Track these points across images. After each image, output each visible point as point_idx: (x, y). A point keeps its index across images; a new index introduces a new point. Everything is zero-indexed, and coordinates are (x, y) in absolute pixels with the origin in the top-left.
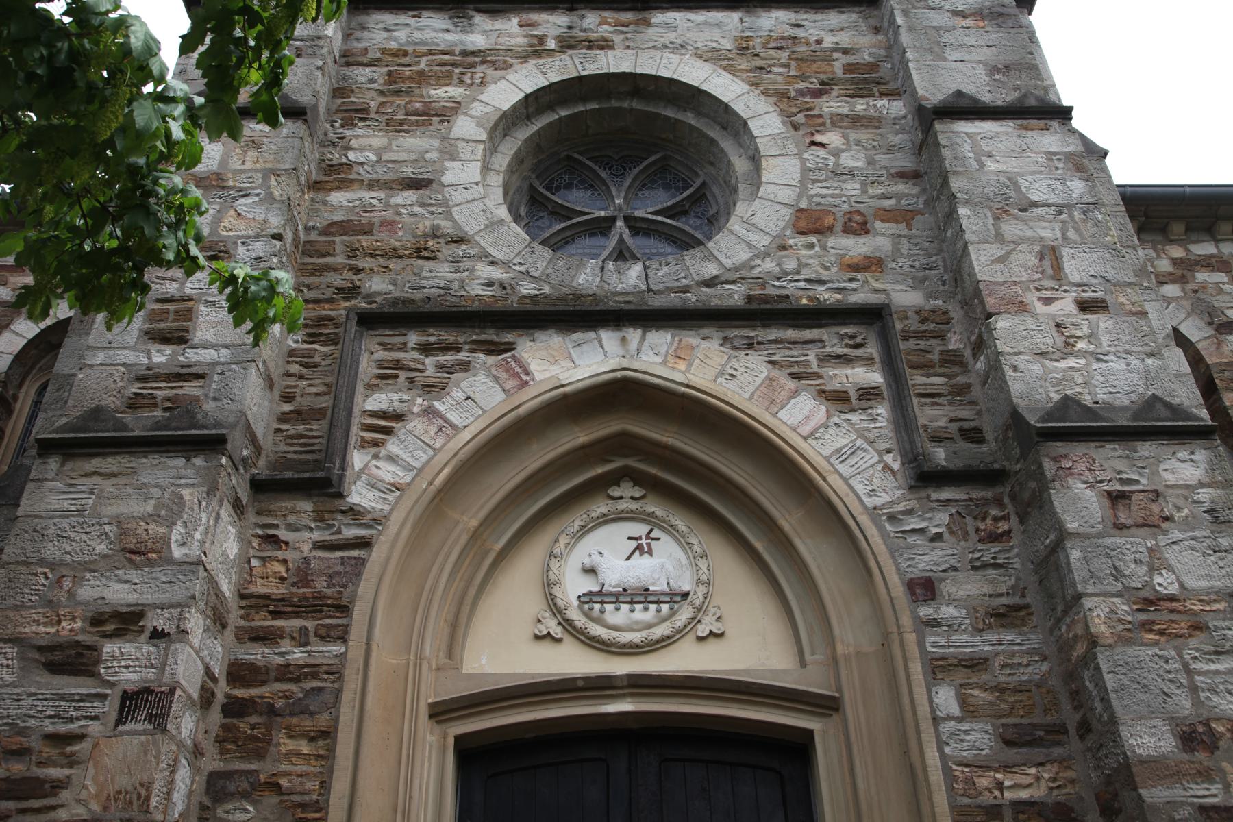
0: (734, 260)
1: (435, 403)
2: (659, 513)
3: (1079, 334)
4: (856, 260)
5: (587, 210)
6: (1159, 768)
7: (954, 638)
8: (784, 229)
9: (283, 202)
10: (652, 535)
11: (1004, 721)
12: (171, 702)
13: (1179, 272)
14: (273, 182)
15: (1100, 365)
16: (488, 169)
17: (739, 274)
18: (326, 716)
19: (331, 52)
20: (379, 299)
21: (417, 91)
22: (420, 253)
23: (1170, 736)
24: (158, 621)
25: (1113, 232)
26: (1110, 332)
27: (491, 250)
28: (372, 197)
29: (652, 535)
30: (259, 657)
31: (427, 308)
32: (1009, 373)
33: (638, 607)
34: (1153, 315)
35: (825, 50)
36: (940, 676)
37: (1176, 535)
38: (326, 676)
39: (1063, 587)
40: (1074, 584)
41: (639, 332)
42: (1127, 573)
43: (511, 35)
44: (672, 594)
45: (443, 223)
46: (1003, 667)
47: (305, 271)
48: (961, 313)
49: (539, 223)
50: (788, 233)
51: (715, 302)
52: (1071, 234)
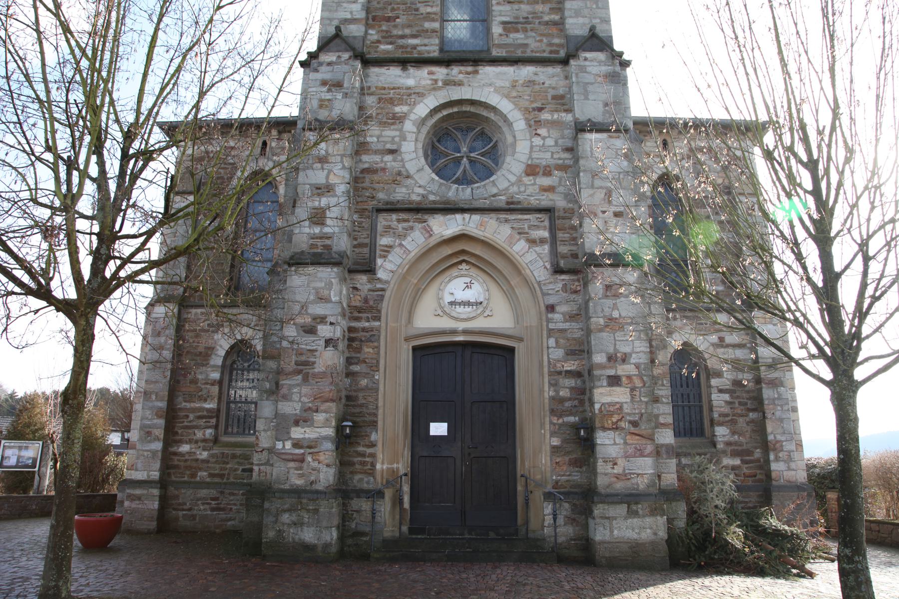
6: (602, 367)
28: (377, 158)
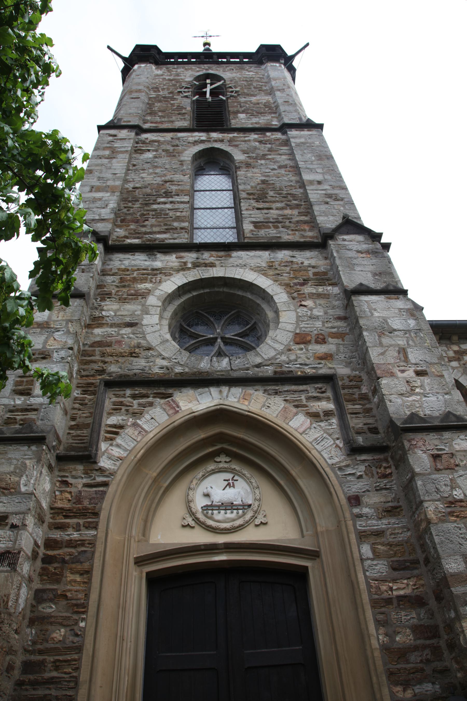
0: (268, 356)
1: (138, 421)
2: (237, 468)
3: (416, 385)
4: (321, 355)
5: (205, 335)
7: (369, 522)
8: (290, 342)
9: (74, 334)
10: (235, 478)
11: (392, 559)
12: (19, 557)
13: (457, 356)
14: (70, 325)
15: (426, 398)
16: (162, 318)
17: (270, 362)
18: (88, 563)
19: (97, 270)
20: (114, 375)
21: (132, 286)
22: (132, 354)
23: (463, 563)
24: (14, 520)
25: (428, 341)
26: (429, 384)
27: (163, 353)
29: (235, 478)
30: (58, 536)
31: (135, 378)
32: (388, 403)
33: (229, 512)
34: (446, 376)
35: (305, 266)
36: (363, 540)
37: (461, 473)
38: (88, 545)
39: (415, 498)
40: (419, 496)
41: (227, 388)
42: (442, 490)
43: (172, 262)
44: (243, 505)
45: (142, 342)
46: (391, 534)
47: (83, 363)
48: (367, 377)
49: (184, 341)
50: (291, 344)
51: (260, 374)
52: (411, 342)
